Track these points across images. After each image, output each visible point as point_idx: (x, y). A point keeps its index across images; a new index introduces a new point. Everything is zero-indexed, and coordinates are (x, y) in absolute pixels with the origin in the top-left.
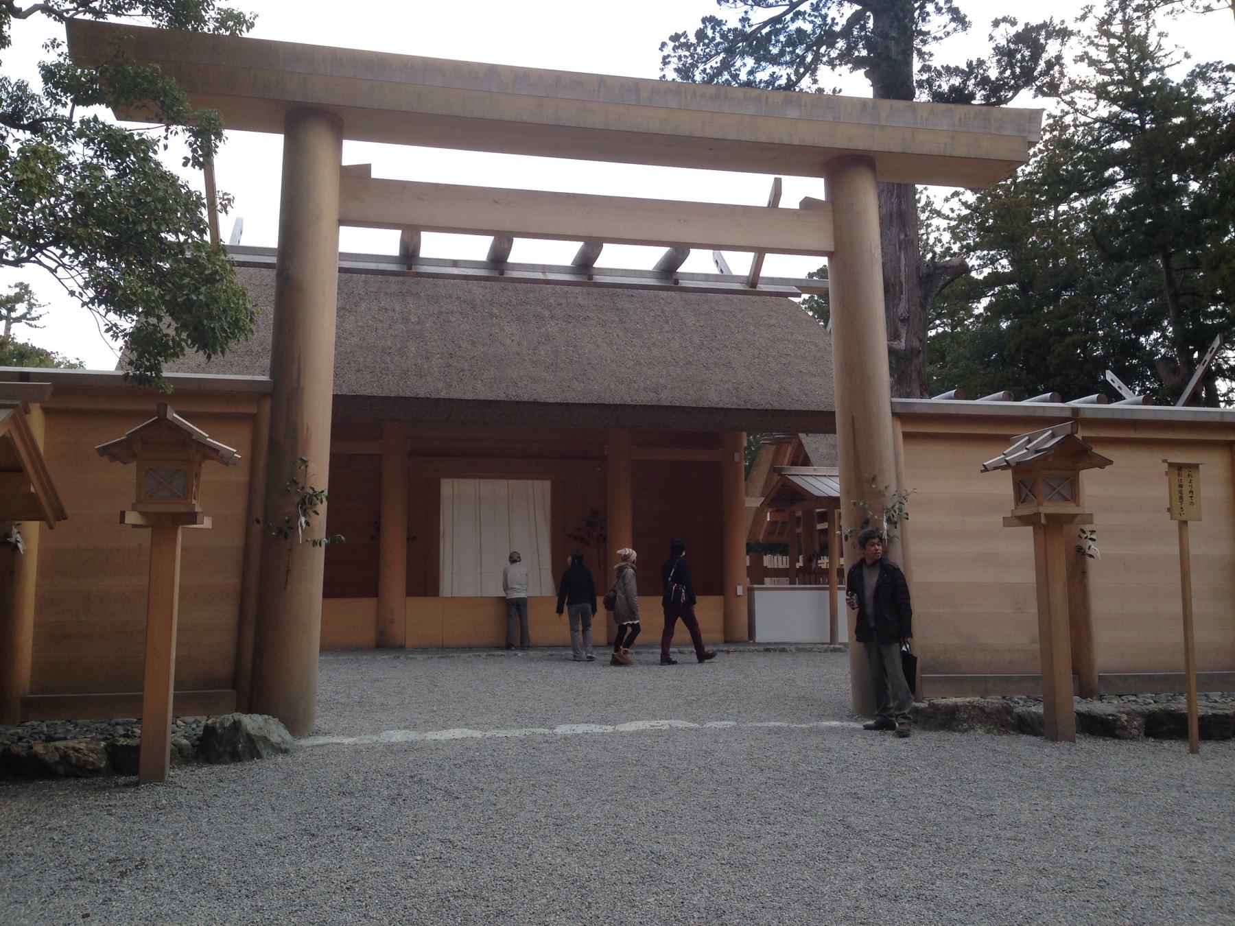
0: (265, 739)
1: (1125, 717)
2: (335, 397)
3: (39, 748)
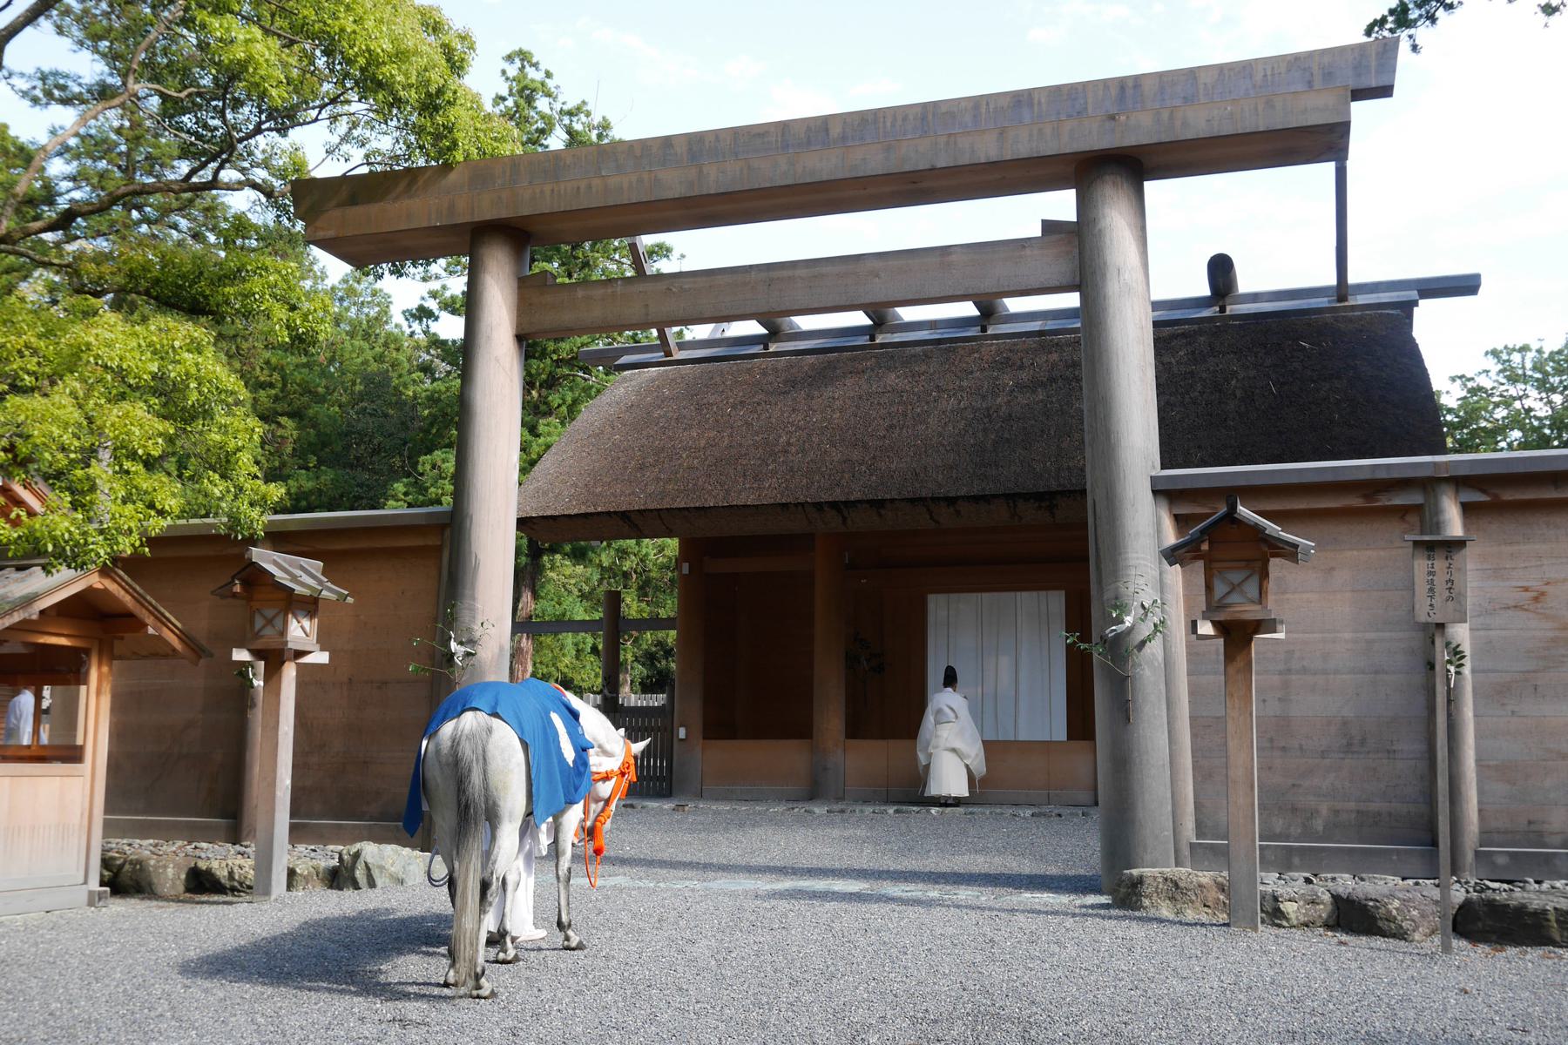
0: (382, 868)
1: (1397, 903)
2: (522, 523)
3: (215, 865)
